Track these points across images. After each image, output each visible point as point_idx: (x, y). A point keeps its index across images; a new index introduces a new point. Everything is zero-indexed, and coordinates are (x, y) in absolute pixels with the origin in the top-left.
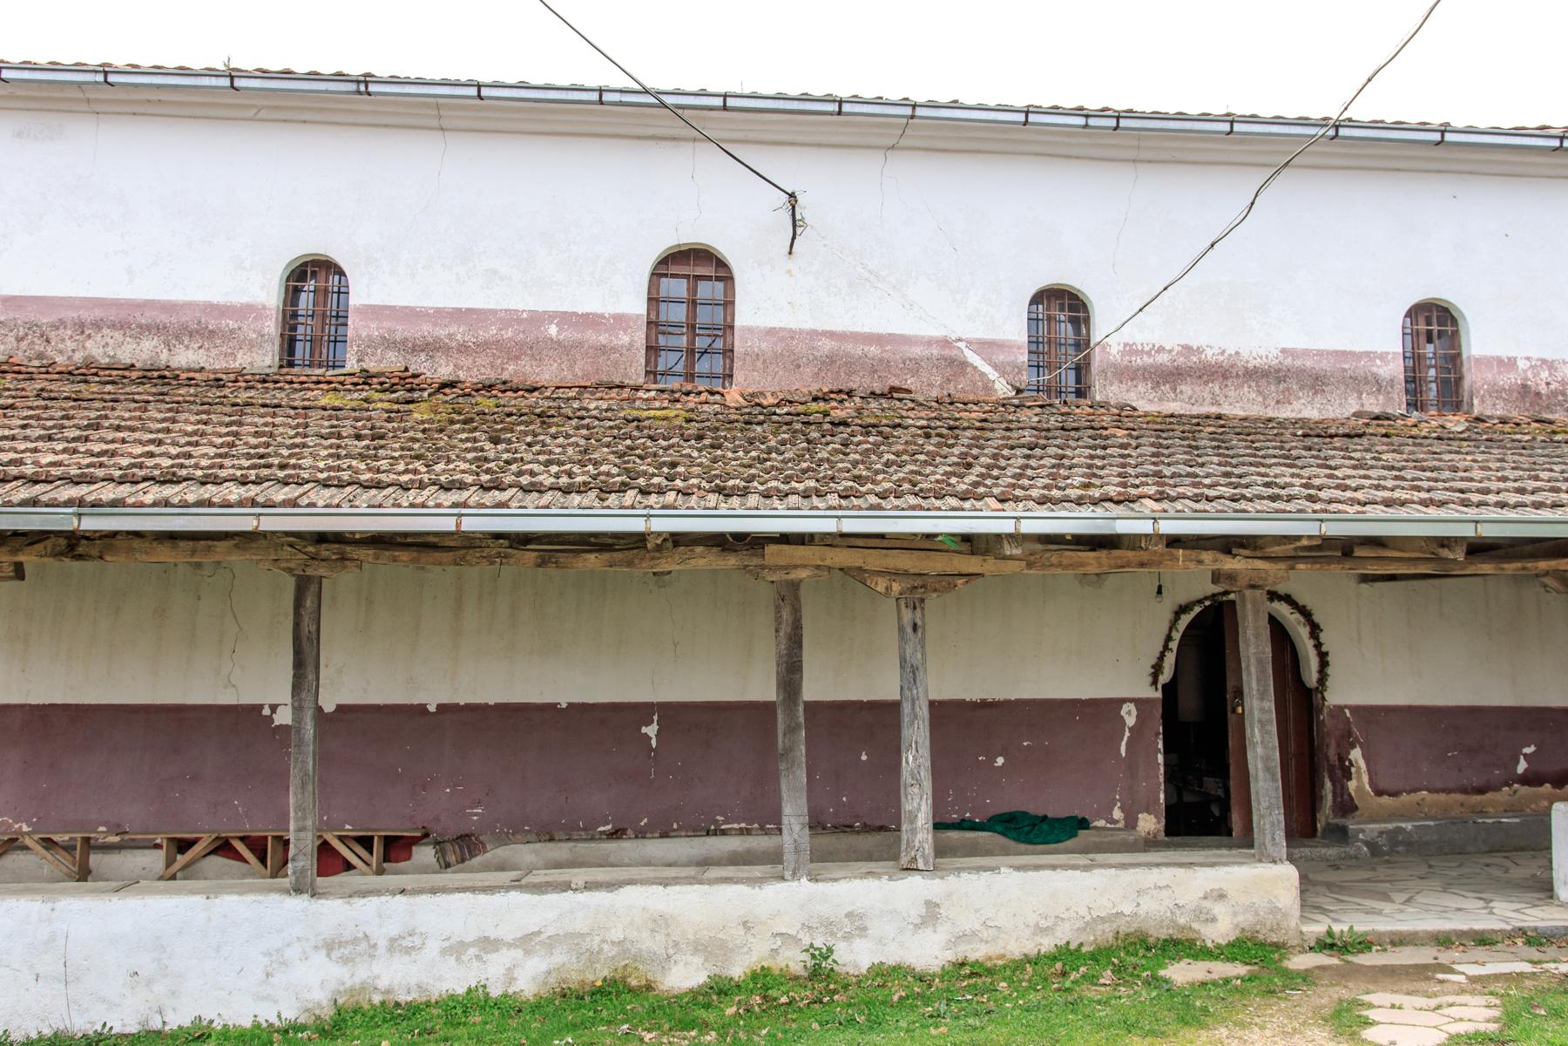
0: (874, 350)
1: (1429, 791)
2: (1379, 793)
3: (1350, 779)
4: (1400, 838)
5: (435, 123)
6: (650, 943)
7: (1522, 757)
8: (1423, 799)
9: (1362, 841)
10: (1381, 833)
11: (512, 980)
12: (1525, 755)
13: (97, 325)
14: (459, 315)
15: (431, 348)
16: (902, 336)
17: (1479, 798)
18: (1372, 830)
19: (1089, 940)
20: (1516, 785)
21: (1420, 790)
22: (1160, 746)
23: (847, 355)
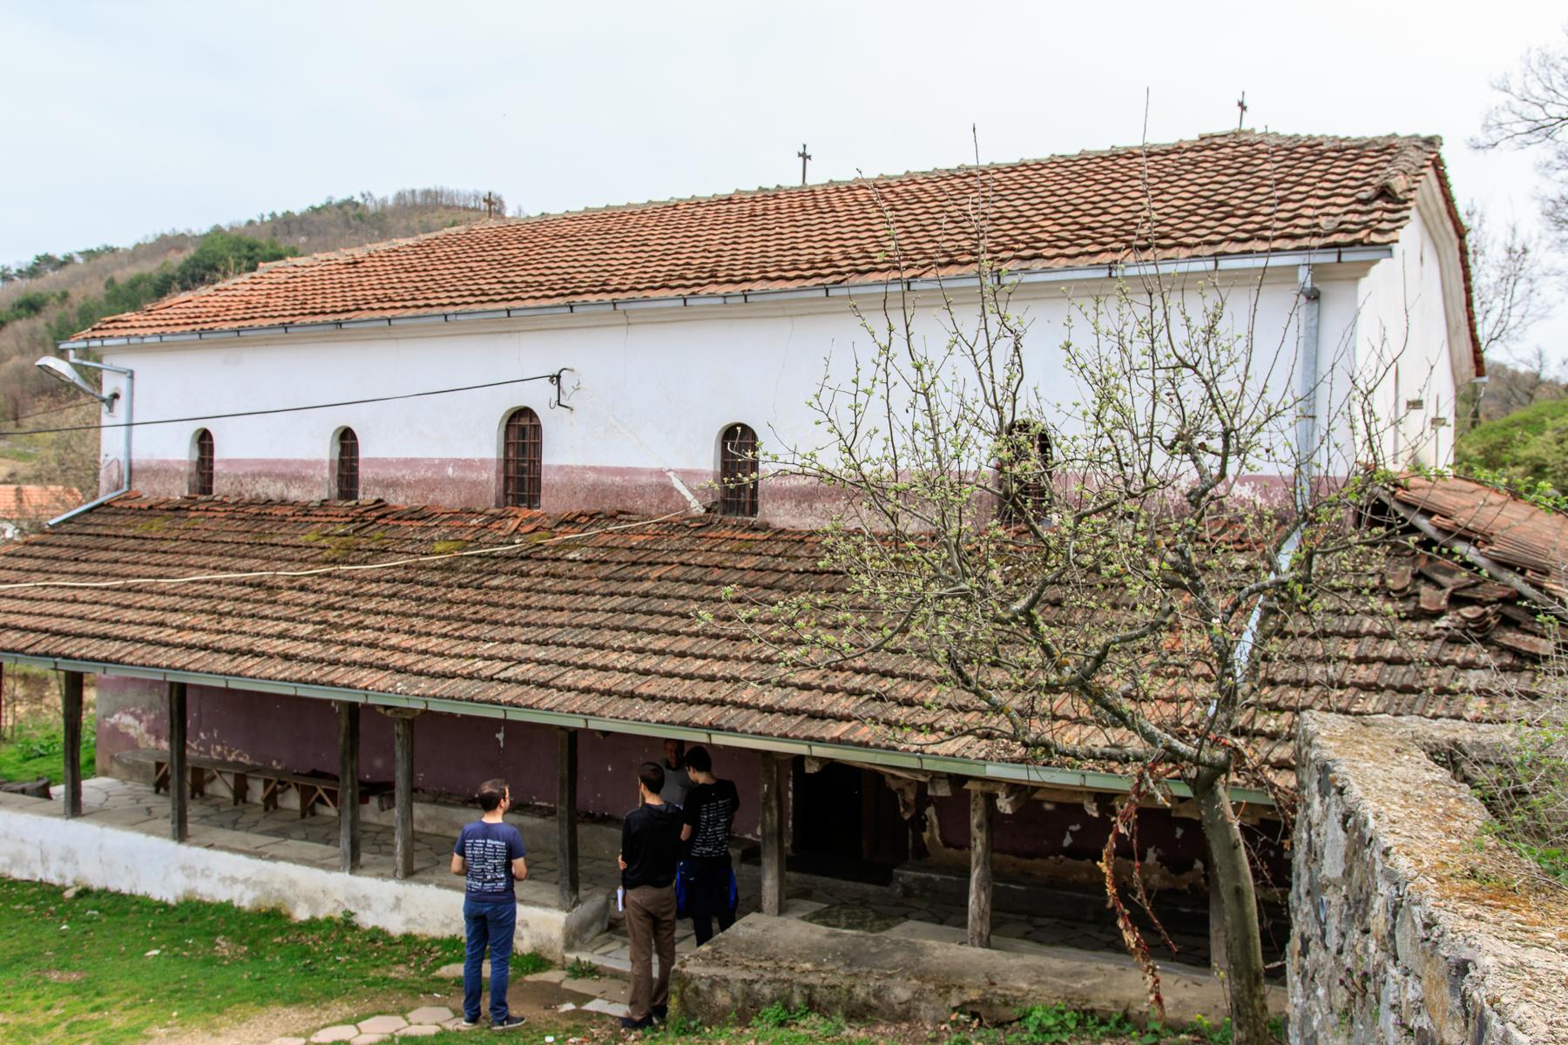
0: (618, 479)
2: (947, 844)
3: (924, 830)
6: (289, 893)
10: (916, 879)
11: (241, 900)
12: (1071, 832)
13: (260, 475)
14: (408, 463)
15: (393, 484)
17: (1028, 862)
22: (791, 785)
23: (603, 484)
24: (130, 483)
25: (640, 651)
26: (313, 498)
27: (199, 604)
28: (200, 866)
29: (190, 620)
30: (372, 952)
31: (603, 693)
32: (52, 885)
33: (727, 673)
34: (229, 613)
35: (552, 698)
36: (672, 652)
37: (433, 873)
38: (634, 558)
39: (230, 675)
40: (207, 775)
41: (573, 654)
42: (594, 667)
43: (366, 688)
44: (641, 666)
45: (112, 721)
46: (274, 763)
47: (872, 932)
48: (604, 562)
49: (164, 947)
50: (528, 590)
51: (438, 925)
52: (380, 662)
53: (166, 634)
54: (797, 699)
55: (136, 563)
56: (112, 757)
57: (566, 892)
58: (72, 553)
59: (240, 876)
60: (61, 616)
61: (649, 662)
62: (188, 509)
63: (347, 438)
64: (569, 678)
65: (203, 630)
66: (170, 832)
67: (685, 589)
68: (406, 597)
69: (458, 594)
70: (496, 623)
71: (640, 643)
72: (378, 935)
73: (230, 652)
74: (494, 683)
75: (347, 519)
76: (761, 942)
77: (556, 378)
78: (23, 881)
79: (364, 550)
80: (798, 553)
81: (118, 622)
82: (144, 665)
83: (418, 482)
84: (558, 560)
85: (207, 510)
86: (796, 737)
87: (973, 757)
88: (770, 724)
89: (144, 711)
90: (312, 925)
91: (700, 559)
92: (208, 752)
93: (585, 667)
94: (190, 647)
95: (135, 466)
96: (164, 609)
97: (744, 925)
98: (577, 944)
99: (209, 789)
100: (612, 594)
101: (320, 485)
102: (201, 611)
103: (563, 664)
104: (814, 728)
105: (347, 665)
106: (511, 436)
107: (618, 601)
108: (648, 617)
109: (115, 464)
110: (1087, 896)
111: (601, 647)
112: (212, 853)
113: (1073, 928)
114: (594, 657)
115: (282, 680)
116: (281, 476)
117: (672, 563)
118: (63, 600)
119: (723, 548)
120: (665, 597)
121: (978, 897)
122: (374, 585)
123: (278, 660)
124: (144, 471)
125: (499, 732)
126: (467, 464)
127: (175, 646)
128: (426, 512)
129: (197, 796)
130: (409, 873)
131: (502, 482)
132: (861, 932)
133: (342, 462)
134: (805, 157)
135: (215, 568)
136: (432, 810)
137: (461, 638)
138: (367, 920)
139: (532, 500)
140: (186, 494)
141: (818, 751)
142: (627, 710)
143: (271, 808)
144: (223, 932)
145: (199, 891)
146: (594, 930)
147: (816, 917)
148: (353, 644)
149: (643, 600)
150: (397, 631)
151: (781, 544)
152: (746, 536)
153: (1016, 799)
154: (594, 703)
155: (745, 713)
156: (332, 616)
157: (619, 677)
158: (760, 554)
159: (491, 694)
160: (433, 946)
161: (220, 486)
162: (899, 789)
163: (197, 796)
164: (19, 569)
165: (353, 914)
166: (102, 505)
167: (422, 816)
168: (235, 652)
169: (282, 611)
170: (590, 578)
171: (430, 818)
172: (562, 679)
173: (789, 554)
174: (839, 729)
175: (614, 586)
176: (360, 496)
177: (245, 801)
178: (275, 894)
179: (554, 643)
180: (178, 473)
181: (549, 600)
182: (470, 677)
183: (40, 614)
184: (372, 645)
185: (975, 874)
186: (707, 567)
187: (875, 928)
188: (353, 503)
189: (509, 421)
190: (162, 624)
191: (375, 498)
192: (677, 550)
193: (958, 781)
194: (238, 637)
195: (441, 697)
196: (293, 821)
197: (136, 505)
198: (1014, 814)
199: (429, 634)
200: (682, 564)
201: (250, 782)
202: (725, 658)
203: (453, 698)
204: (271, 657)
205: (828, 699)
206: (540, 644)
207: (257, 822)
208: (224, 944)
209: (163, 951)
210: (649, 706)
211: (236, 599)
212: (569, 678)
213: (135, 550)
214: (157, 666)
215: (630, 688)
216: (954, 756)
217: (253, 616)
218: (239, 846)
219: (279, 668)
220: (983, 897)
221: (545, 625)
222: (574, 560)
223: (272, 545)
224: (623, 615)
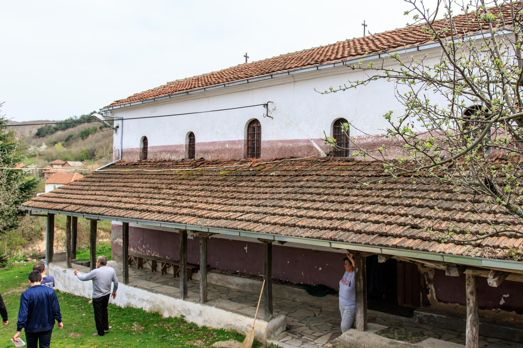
0: (291, 145)
1: (460, 304)
2: (439, 301)
3: (428, 294)
4: (432, 319)
5: (204, 96)
6: (162, 306)
7: (502, 298)
8: (457, 307)
9: (417, 317)
10: (425, 316)
12: (504, 298)
14: (213, 143)
15: (207, 152)
16: (298, 140)
18: (422, 314)
19: (226, 329)
20: (499, 309)
21: (456, 303)
23: (285, 147)
24: (122, 157)
25: (298, 208)
26: (180, 159)
27: (134, 195)
28: (132, 294)
29: (130, 200)
30: (189, 333)
31: (281, 225)
32: (86, 298)
33: (339, 217)
34: (143, 197)
35: (259, 227)
36: (313, 208)
37: (215, 301)
38: (297, 174)
39: (139, 219)
40: (143, 261)
41: (269, 210)
42: (279, 214)
43: (186, 223)
44: (299, 214)
45: (116, 241)
46: (167, 257)
47: (412, 343)
48: (285, 176)
49: (114, 325)
50: (254, 186)
51: (216, 323)
52: (193, 213)
53: (122, 205)
54: (372, 228)
55: (118, 182)
56: (115, 253)
57: (267, 313)
58: (99, 180)
59: (145, 299)
60: (90, 199)
61: (303, 212)
62: (138, 164)
63: (191, 136)
64: (268, 219)
65: (133, 203)
66: (122, 280)
67: (318, 184)
68: (207, 190)
69: (227, 189)
70: (240, 199)
71: (298, 205)
72: (193, 326)
73: (140, 211)
74: (236, 221)
75: (190, 165)
76: (357, 344)
77: (266, 105)
78: (77, 296)
79: (194, 175)
80: (368, 169)
81: (106, 201)
82: (111, 216)
83: (216, 151)
84: (266, 175)
85: (144, 164)
86: (373, 245)
87: (473, 256)
88: (360, 239)
90: (169, 320)
91: (324, 173)
92: (145, 252)
93: (274, 214)
94: (127, 209)
95: (123, 151)
96: (122, 197)
97: (348, 334)
98: (272, 336)
99: (144, 266)
100: (287, 187)
101: (182, 154)
102: (134, 197)
103: (265, 213)
104: (383, 241)
105: (180, 215)
106: (250, 131)
107: (289, 189)
108: (302, 195)
109: (117, 150)
110: (515, 329)
111: (282, 207)
112: (136, 289)
113: (510, 345)
114: (279, 211)
115: (156, 221)
116: (169, 152)
117: (313, 175)
118: (92, 194)
119: (334, 168)
120: (310, 187)
121: (472, 330)
122: (196, 187)
123: (156, 213)
124: (126, 152)
125: (246, 247)
126: (234, 142)
127: (122, 209)
128: (218, 161)
129: (140, 268)
130: (205, 301)
131: (246, 149)
132: (407, 343)
133: (190, 145)
134: (365, 25)
135: (143, 183)
136: (220, 276)
137: (225, 204)
138: (189, 319)
139: (258, 155)
140: (139, 160)
141: (385, 251)
142: (292, 232)
143: (164, 274)
144: (137, 321)
145: (132, 303)
146: (280, 330)
147: (382, 333)
148: (184, 207)
149: (300, 188)
150: (202, 202)
151: (360, 166)
152: (344, 164)
153: (499, 279)
154: (277, 229)
155: (347, 233)
156: (178, 198)
157: (289, 218)
158: (351, 170)
159: (234, 225)
160: (213, 332)
161: (150, 156)
162: (425, 273)
163: (140, 268)
164: (82, 185)
165: (184, 317)
166: (112, 164)
167: (217, 279)
168: (142, 211)
169: (161, 196)
170: (279, 181)
171: (219, 280)
172: (264, 219)
173: (364, 169)
174: (396, 241)
175: (288, 184)
176: (196, 157)
177: (156, 271)
178: (157, 306)
179: (262, 206)
180: (137, 152)
181: (262, 190)
182: (227, 219)
183: (83, 199)
184: (191, 207)
185: (469, 318)
186: (327, 176)
187: (413, 341)
188: (193, 159)
189: (249, 125)
190: (120, 201)
191: (201, 157)
192: (315, 170)
193: (462, 268)
194: (144, 206)
195: (214, 227)
196: (171, 278)
197: (122, 164)
198: (498, 287)
199: (213, 203)
200: (317, 175)
201: (158, 264)
202: (337, 210)
203: (219, 227)
204: (154, 212)
205: (388, 228)
206: (256, 206)
207: (158, 278)
208: (136, 325)
209: (113, 327)
210: (302, 230)
211: (147, 193)
212: (268, 219)
213: (119, 178)
214: (115, 216)
215: (294, 223)
216: (462, 255)
217: (151, 198)
218: (145, 287)
219: (156, 216)
220: (474, 330)
221: (259, 199)
222: (273, 176)
223: (163, 175)
224: (291, 194)
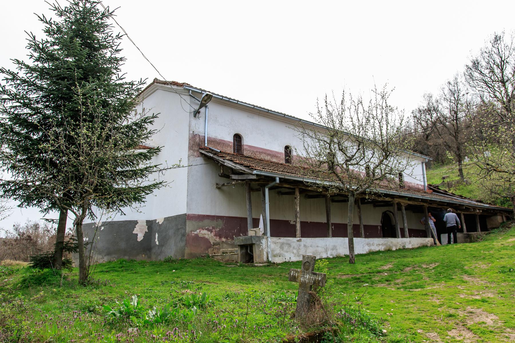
6: (391, 245)
13: (262, 153)
45: (196, 233)
59: (381, 243)
89: (213, 228)
116: (269, 155)
